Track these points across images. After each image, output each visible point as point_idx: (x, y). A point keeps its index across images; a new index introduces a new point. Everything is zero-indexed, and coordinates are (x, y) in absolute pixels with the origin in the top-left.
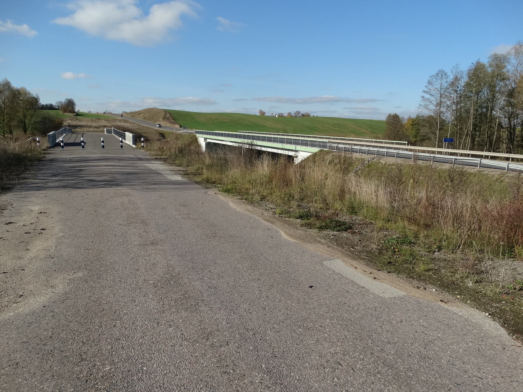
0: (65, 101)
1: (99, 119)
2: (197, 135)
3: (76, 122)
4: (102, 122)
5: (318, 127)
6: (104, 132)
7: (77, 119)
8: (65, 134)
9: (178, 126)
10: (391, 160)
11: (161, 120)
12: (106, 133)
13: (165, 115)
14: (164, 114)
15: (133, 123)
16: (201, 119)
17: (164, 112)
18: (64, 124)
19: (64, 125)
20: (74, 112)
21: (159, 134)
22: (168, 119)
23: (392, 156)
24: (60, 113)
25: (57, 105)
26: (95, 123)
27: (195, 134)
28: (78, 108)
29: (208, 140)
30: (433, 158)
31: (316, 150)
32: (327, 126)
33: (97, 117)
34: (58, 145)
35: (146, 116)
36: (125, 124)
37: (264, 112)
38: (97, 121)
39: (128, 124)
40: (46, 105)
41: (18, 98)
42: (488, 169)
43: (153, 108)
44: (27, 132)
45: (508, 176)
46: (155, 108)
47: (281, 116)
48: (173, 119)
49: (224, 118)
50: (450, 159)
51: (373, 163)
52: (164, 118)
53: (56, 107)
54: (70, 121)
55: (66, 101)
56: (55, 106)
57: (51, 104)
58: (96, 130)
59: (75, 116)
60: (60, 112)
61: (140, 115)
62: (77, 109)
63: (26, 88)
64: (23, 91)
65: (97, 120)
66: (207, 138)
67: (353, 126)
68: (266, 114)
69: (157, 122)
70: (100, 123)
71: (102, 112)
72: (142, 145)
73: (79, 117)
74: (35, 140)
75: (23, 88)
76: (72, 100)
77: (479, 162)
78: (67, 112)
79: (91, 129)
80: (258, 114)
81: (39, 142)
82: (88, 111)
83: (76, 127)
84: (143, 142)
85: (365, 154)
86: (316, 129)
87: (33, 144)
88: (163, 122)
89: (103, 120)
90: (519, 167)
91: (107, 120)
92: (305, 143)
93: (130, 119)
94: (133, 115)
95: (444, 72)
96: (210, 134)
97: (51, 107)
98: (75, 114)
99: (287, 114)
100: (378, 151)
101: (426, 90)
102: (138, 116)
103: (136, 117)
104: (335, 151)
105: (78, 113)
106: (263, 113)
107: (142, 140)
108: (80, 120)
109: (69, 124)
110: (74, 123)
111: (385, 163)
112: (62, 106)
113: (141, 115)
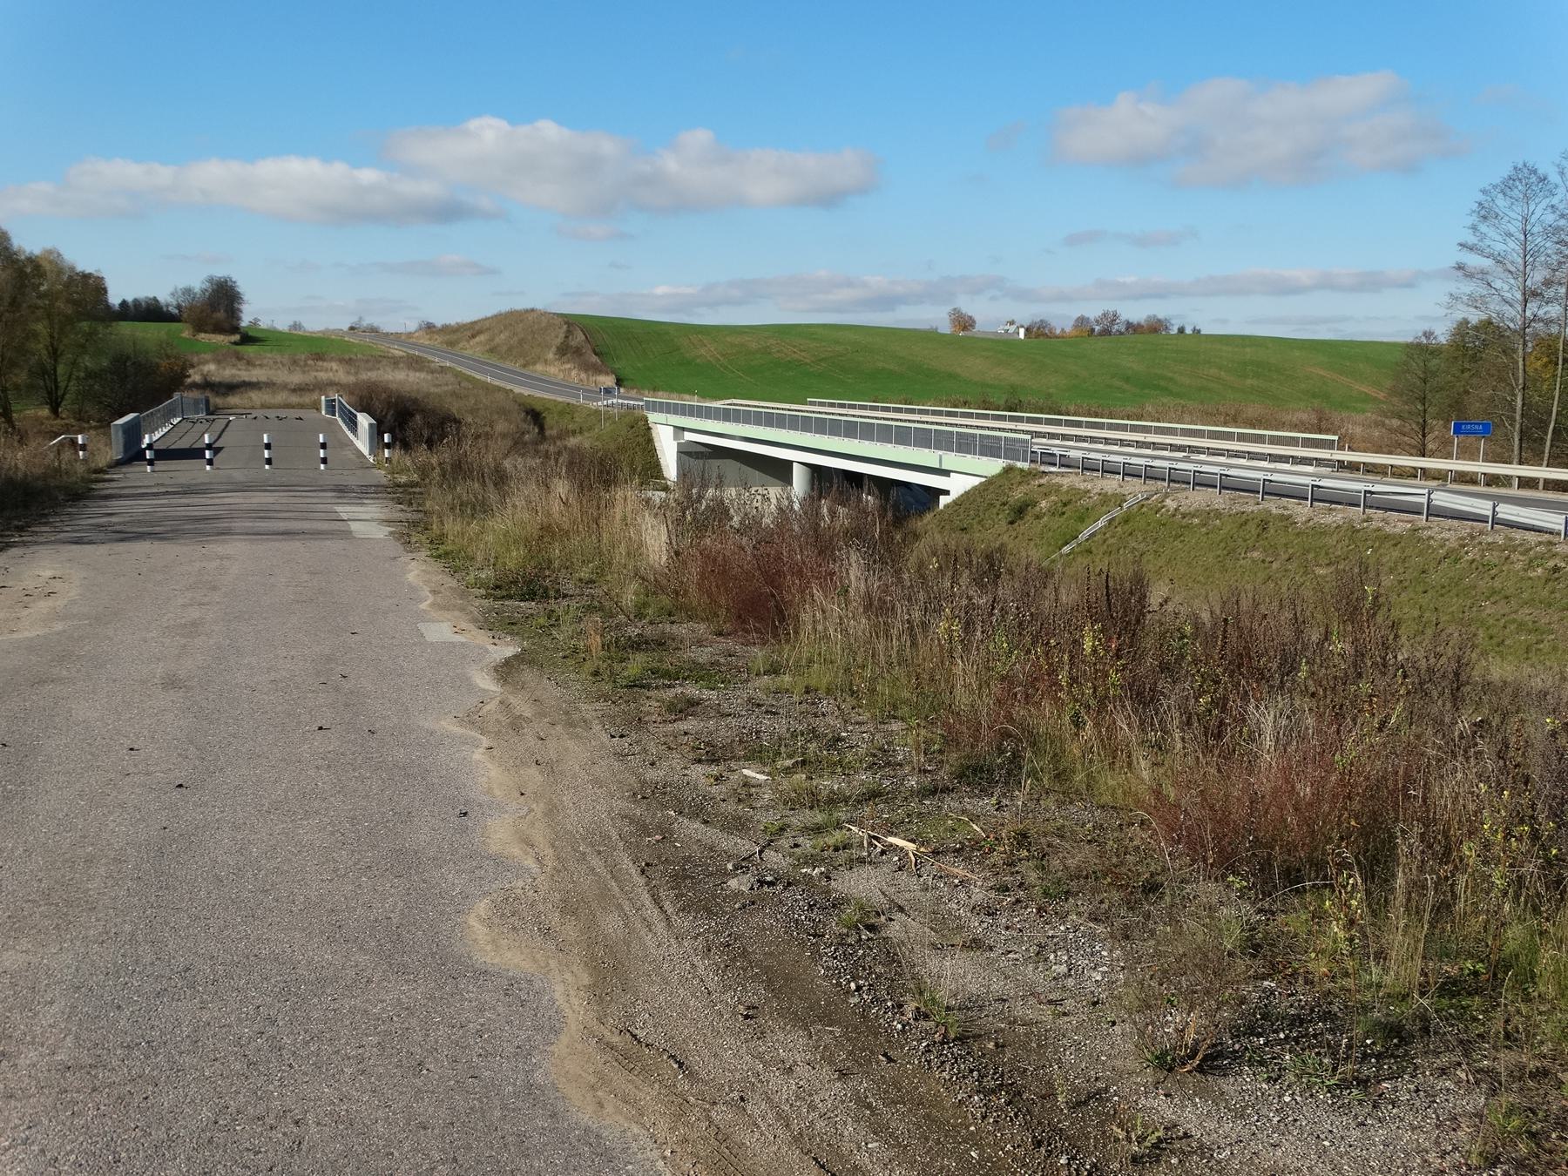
0: (204, 286)
1: (319, 357)
2: (653, 417)
3: (234, 371)
4: (326, 370)
5: (1171, 379)
6: (319, 410)
7: (239, 358)
8: (179, 419)
9: (608, 381)
10: (1197, 499)
11: (551, 356)
12: (323, 412)
13: (566, 337)
14: (562, 335)
15: (443, 370)
16: (703, 351)
17: (565, 327)
18: (189, 376)
19: (189, 380)
20: (235, 329)
21: (523, 414)
22: (578, 352)
23: (1201, 482)
24: (184, 335)
25: (175, 303)
26: (304, 372)
27: (645, 413)
28: (256, 310)
29: (689, 436)
30: (1365, 496)
31: (993, 466)
32: (1213, 371)
33: (317, 348)
34: (140, 456)
35: (497, 340)
36: (412, 374)
37: (970, 317)
38: (310, 366)
39: (423, 375)
40: (136, 302)
41: (36, 287)
42: (1456, 523)
43: (527, 311)
44: (60, 410)
45: (1480, 543)
46: (533, 310)
47: (1037, 331)
48: (596, 354)
49: (795, 347)
50: (1289, 483)
51: (1145, 509)
52: (563, 351)
53: (170, 308)
54: (212, 367)
55: (207, 285)
56: (167, 306)
57: (155, 299)
58: (294, 399)
59: (235, 343)
60: (182, 332)
61: (477, 339)
62: (248, 315)
63: (61, 252)
64: (51, 262)
65: (310, 362)
66: (684, 429)
67: (1322, 373)
68: (978, 327)
69: (534, 363)
70: (321, 371)
71: (345, 327)
72: (386, 456)
73: (249, 350)
74: (73, 442)
75: (50, 252)
76: (229, 283)
77: (1424, 500)
78: (206, 332)
79: (281, 397)
80: (946, 328)
81: (83, 447)
82: (292, 323)
83: (231, 388)
84: (388, 446)
85: (1135, 479)
86: (1162, 383)
87: (67, 455)
88: (556, 363)
89: (332, 359)
90: (1521, 514)
91: (349, 361)
92: (965, 445)
93: (434, 355)
94: (454, 337)
95: (1535, 172)
96: (699, 415)
97: (150, 312)
98: (237, 337)
99: (1072, 323)
100: (1198, 472)
101: (1471, 239)
102: (468, 341)
103: (461, 345)
104: (1053, 469)
105: (250, 334)
106: (964, 322)
107: (386, 441)
108: (250, 363)
109: (205, 377)
110: (228, 373)
111: (1176, 510)
112: (191, 308)
113: (482, 338)
